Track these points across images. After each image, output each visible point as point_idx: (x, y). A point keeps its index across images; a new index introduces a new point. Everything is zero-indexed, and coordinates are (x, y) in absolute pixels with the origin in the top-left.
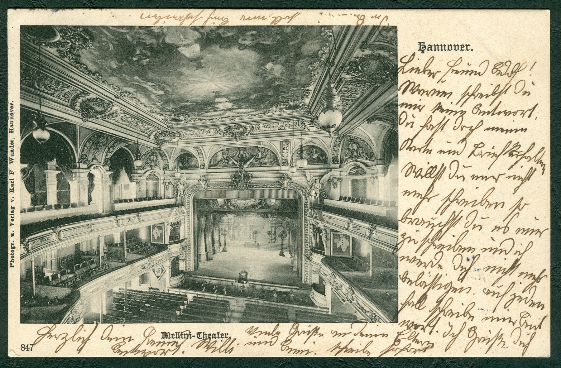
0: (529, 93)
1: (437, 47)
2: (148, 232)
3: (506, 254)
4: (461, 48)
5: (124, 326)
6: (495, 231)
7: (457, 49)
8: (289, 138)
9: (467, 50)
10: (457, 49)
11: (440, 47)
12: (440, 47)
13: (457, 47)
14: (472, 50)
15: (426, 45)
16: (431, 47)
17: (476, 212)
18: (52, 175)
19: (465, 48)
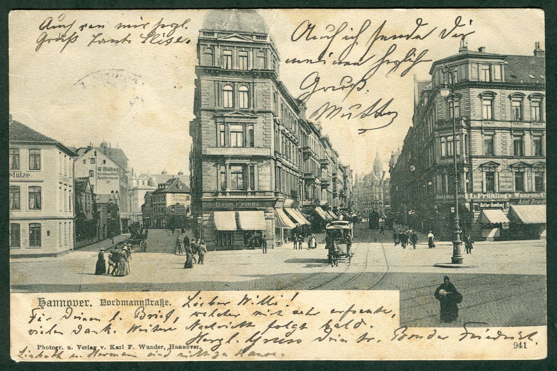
0: (186, 328)
1: (56, 303)
2: (48, 146)
3: (76, 334)
4: (81, 303)
5: (65, 156)
6: (131, 331)
7: (76, 304)
8: (19, 146)
9: (86, 305)
10: (76, 304)
11: (59, 303)
12: (59, 303)
13: (76, 303)
14: (91, 306)
15: (46, 301)
16: (51, 303)
17: (395, 114)
18: (451, 83)
19: (84, 304)
